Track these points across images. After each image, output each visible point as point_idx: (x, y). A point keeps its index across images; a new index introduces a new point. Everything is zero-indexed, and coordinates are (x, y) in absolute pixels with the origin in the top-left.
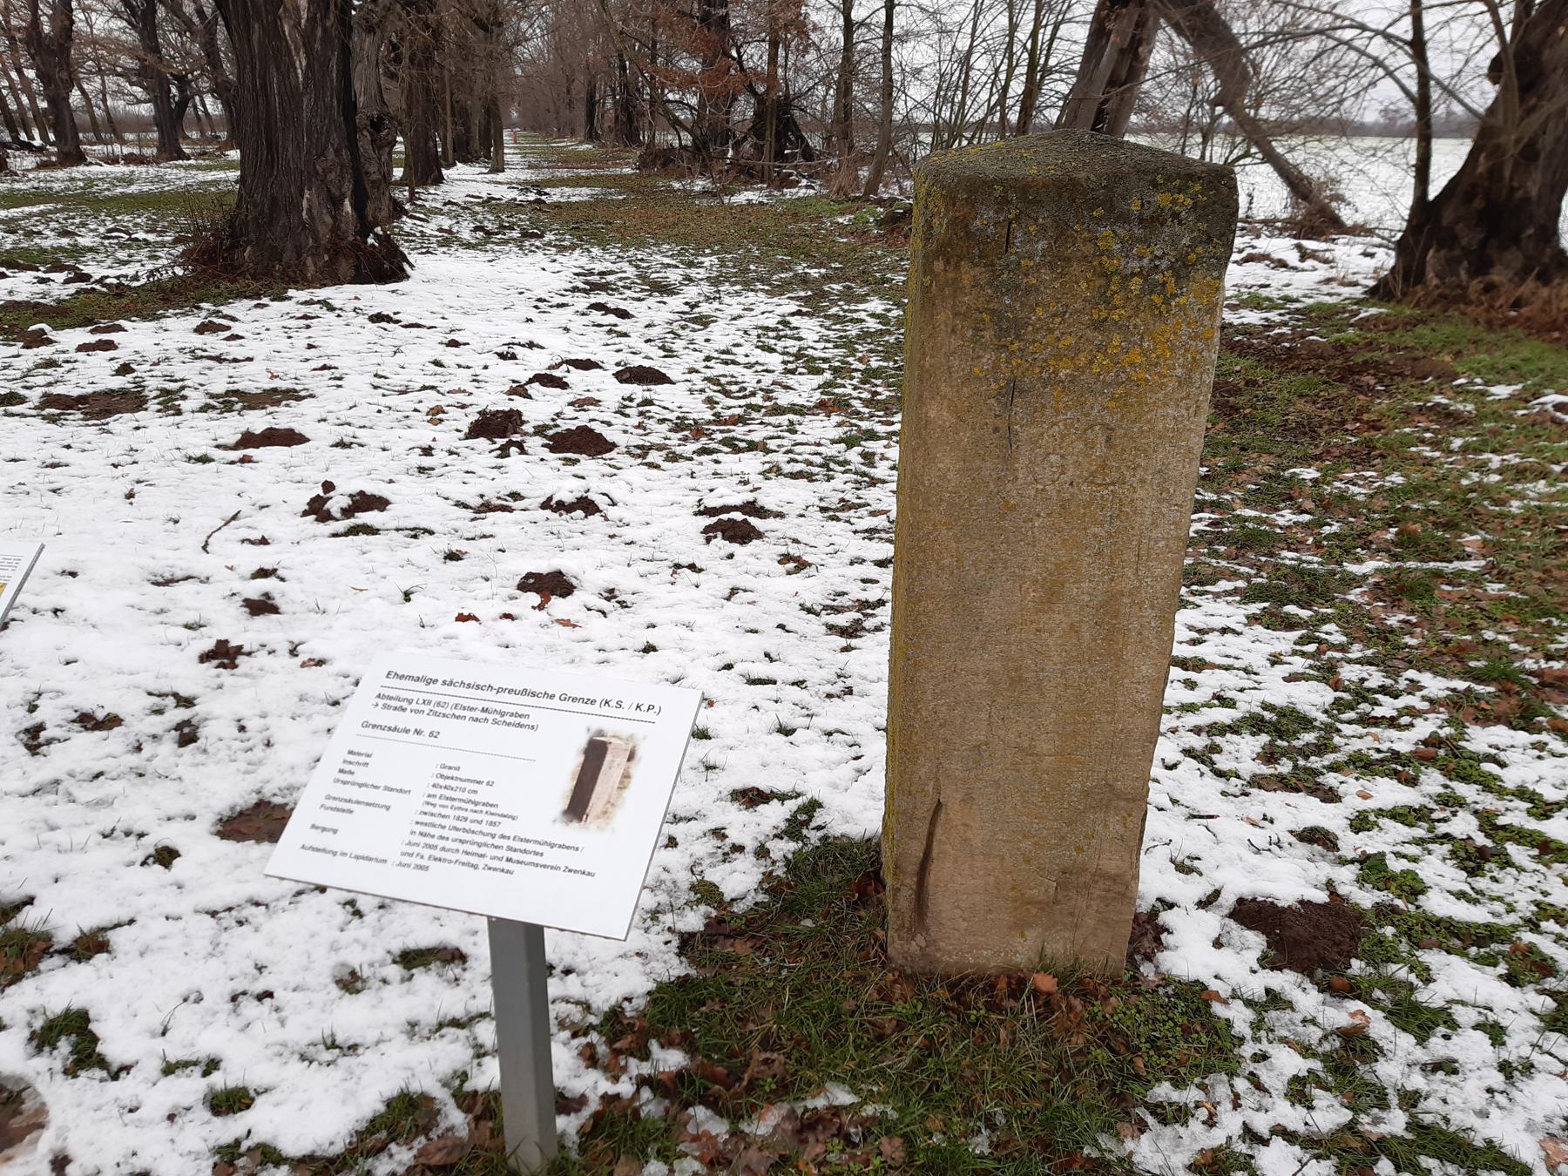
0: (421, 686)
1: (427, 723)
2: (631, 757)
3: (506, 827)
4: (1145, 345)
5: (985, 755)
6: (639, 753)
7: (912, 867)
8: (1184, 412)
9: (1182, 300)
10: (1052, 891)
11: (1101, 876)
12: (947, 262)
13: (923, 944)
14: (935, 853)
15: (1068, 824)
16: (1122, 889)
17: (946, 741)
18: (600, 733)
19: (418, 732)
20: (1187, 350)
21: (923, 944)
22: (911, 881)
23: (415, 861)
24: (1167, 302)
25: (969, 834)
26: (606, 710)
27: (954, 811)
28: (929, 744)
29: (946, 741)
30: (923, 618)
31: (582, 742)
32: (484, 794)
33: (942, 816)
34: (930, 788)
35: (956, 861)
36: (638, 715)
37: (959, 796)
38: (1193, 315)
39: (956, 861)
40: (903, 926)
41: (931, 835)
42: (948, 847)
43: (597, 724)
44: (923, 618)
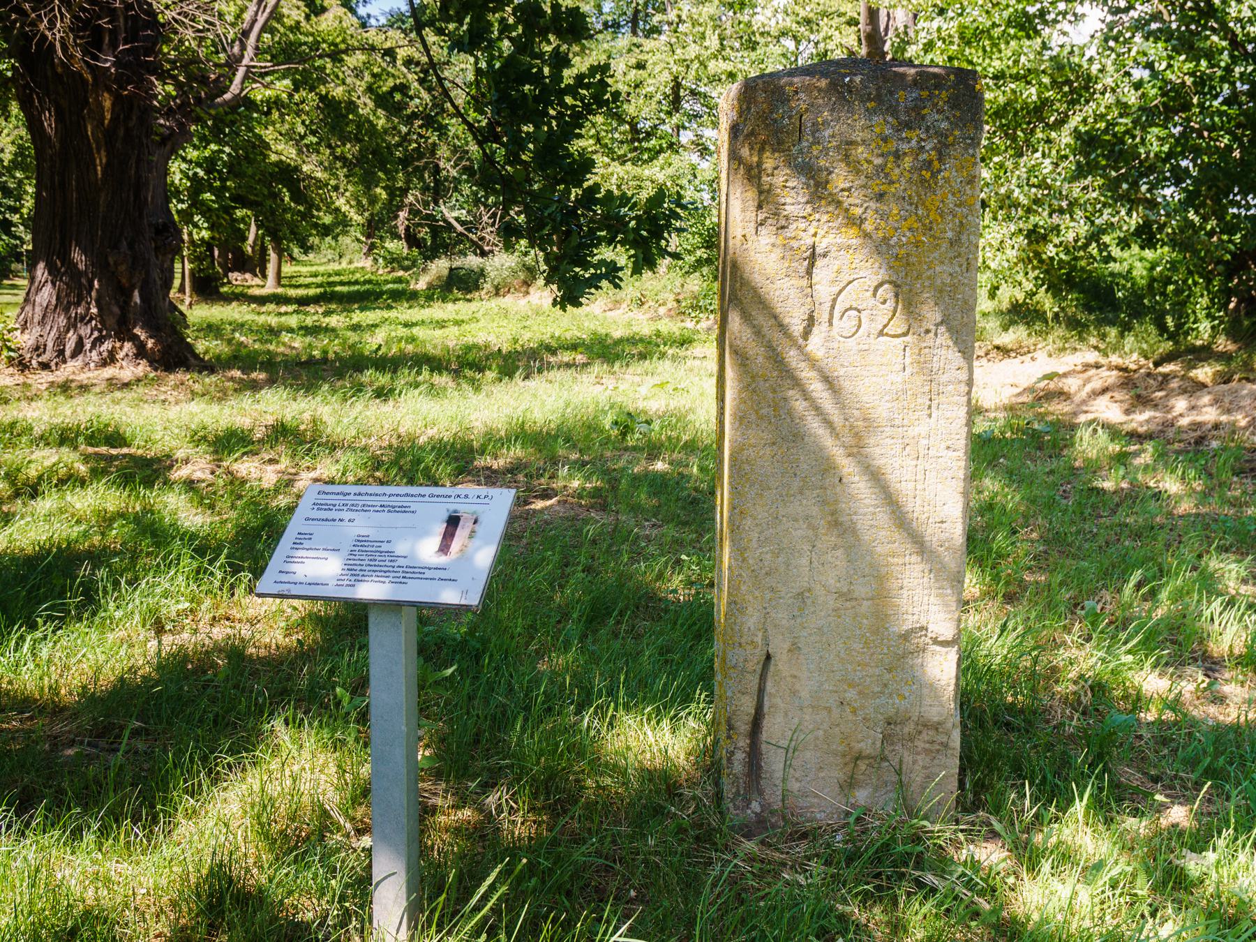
0: (341, 497)
1: (346, 515)
2: (475, 522)
3: (401, 562)
4: (920, 212)
5: (809, 602)
6: (480, 520)
7: (743, 726)
8: (957, 269)
9: (946, 174)
10: (879, 744)
11: (925, 726)
12: (751, 149)
13: (758, 810)
14: (766, 709)
15: (889, 671)
16: (945, 740)
17: (772, 590)
18: (455, 511)
19: (341, 520)
20: (954, 216)
21: (758, 810)
22: (743, 742)
23: (346, 583)
24: (934, 175)
25: (797, 687)
26: (458, 500)
27: (781, 663)
28: (757, 594)
29: (772, 590)
30: (747, 467)
31: (445, 516)
32: (385, 547)
33: (772, 668)
34: (759, 639)
35: (786, 715)
36: (479, 501)
37: (787, 646)
38: (957, 187)
39: (786, 715)
40: (738, 793)
41: (761, 691)
42: (778, 701)
43: (452, 507)
44: (747, 467)
